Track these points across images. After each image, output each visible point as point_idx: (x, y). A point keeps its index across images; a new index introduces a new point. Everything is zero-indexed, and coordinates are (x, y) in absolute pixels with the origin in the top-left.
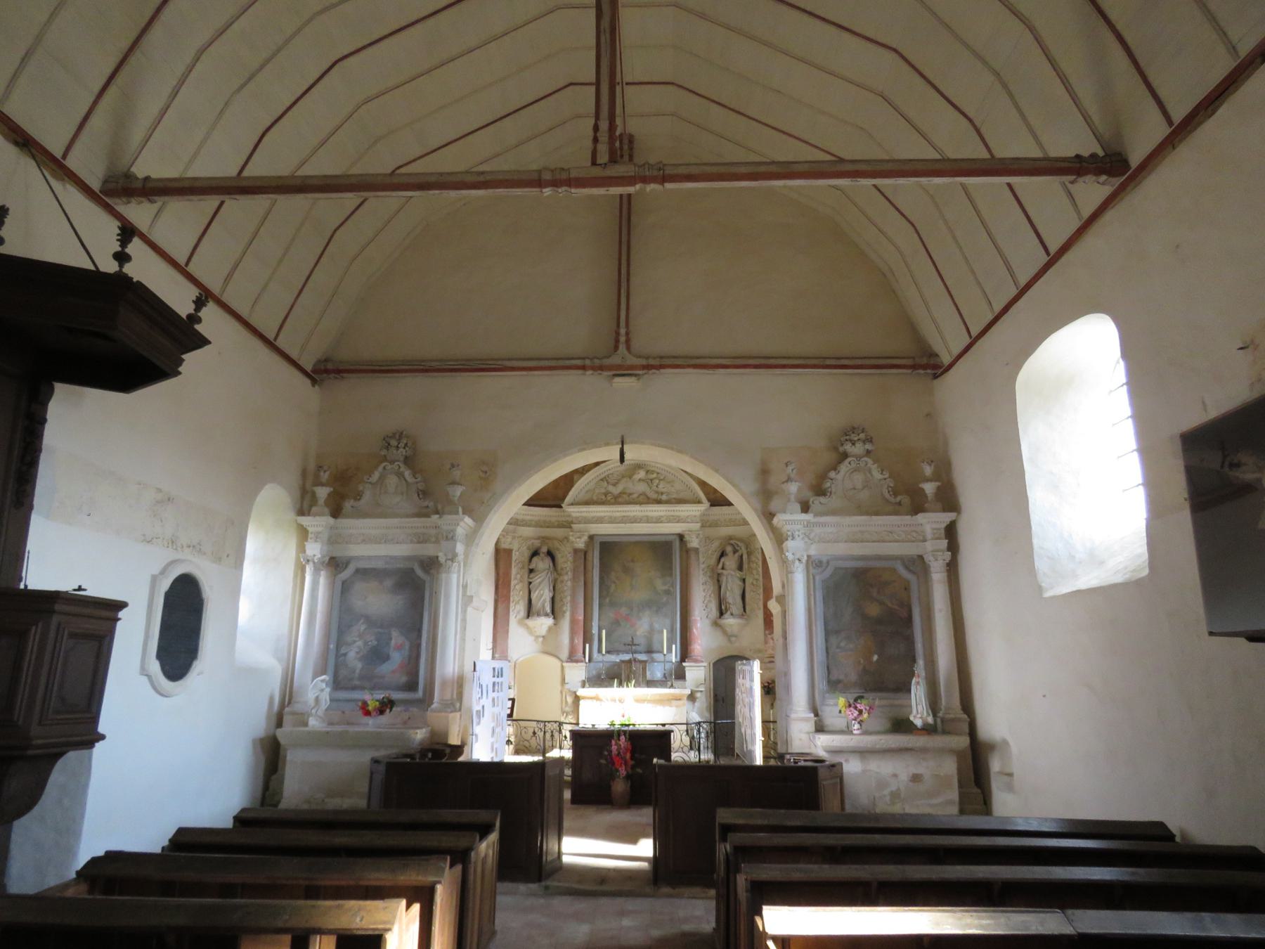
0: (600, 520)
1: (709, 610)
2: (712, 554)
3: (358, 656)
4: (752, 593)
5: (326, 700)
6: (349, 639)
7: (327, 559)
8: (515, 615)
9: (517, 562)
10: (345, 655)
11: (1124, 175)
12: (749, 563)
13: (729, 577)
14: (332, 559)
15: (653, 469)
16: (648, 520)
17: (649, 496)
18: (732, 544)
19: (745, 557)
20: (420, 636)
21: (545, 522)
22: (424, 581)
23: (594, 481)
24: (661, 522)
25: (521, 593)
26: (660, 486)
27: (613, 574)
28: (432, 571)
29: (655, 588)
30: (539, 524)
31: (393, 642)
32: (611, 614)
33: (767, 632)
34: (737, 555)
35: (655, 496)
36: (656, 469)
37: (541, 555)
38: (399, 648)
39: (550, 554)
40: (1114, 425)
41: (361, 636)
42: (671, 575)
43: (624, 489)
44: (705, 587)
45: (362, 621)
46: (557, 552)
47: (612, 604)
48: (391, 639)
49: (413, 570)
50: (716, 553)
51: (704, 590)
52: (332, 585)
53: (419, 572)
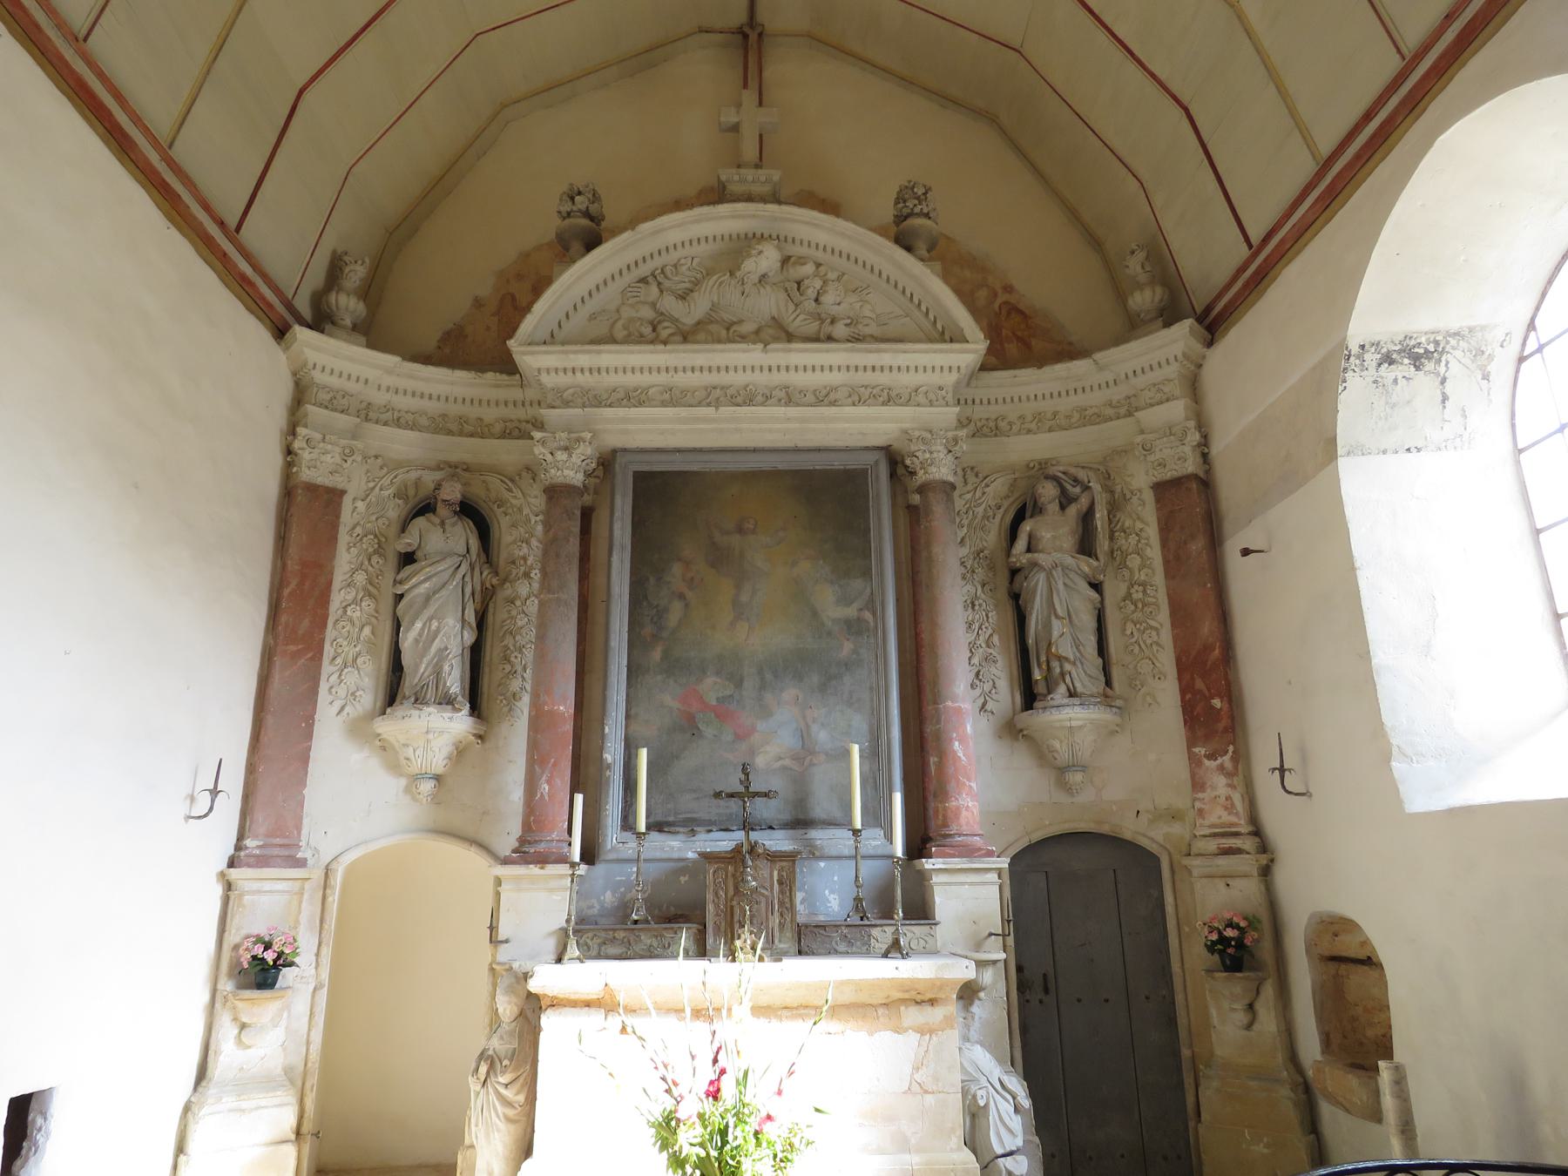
0: (634, 398)
1: (987, 687)
2: (986, 517)
4: (1130, 628)
8: (338, 704)
9: (359, 530)
12: (1112, 538)
13: (1057, 573)
18: (1055, 479)
19: (1100, 516)
21: (462, 420)
23: (621, 283)
24: (833, 403)
25: (367, 631)
26: (828, 299)
27: (677, 569)
29: (815, 614)
30: (441, 426)
32: (668, 698)
33: (1200, 750)
34: (1073, 510)
35: (812, 327)
36: (812, 252)
37: (442, 511)
39: (468, 510)
42: (866, 573)
43: (714, 307)
46: (499, 511)
47: (673, 666)
51: (970, 625)
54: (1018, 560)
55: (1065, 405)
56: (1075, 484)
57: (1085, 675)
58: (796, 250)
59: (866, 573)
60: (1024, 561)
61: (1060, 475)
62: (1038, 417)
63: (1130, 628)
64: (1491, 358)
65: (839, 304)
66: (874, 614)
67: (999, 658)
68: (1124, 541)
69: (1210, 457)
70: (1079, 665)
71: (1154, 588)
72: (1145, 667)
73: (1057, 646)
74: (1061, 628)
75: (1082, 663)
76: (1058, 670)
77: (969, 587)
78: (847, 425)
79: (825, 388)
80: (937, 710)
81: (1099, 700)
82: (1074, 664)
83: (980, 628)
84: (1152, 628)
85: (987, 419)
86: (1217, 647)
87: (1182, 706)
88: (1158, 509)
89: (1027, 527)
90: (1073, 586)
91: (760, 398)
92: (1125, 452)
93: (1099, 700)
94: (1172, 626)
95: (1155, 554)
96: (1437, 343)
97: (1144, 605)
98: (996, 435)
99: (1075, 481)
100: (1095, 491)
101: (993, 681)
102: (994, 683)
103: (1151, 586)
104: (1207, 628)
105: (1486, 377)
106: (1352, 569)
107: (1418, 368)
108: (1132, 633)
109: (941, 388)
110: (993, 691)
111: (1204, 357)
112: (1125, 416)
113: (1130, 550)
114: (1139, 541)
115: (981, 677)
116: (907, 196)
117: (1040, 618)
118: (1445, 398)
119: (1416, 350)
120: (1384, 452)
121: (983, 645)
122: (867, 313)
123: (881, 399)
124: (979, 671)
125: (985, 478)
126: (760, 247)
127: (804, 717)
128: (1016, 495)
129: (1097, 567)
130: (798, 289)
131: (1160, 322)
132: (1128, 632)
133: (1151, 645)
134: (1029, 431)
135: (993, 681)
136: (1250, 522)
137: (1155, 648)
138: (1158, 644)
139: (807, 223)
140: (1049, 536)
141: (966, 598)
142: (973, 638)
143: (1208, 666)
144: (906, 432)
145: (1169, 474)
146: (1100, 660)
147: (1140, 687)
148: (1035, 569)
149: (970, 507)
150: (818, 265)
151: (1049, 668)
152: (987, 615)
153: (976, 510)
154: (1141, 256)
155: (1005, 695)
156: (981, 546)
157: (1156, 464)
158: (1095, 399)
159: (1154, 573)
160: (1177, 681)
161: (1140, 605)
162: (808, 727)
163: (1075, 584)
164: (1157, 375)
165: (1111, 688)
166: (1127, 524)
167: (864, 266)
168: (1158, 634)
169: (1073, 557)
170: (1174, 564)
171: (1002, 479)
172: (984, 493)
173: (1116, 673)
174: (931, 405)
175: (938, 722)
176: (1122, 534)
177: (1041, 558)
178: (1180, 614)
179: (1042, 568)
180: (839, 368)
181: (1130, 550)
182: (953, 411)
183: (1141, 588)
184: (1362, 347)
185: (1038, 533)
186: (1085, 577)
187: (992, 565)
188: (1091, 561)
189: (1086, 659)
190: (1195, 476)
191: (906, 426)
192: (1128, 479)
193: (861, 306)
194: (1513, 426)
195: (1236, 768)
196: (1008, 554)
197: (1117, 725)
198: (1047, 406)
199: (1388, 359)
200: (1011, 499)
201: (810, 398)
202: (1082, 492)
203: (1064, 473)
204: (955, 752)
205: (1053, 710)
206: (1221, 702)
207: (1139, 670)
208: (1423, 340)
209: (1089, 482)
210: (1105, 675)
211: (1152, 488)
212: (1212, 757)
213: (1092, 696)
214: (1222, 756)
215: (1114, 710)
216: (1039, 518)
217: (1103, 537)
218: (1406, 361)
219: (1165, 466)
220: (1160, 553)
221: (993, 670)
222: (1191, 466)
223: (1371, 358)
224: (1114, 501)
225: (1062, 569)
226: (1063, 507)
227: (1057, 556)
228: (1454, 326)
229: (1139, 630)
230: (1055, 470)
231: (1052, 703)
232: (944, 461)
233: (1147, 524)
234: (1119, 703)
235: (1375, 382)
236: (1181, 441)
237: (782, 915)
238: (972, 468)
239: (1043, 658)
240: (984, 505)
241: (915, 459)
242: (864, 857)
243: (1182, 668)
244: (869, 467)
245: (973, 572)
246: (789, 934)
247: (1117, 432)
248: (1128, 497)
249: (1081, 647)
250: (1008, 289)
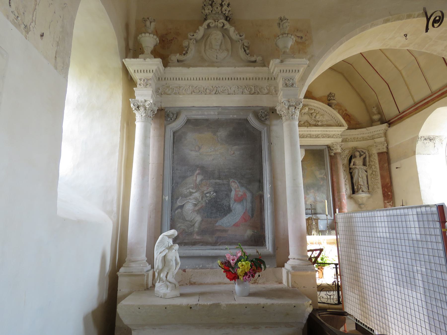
3: (197, 208)
4: (372, 179)
5: (176, 260)
6: (185, 191)
7: (156, 109)
10: (182, 207)
11: (439, 22)
13: (360, 169)
14: (161, 110)
15: (312, 107)
16: (311, 136)
17: (310, 123)
18: (359, 151)
19: (367, 158)
20: (261, 188)
22: (260, 133)
24: (319, 138)
26: (317, 117)
28: (267, 122)
31: (233, 194)
33: (386, 202)
34: (362, 157)
35: (314, 123)
36: (314, 108)
38: (240, 200)
41: (197, 187)
42: (325, 169)
45: (197, 172)
48: (231, 191)
49: (247, 120)
50: (347, 157)
52: (162, 137)
53: (254, 122)
55: (359, 136)
57: (365, 188)
58: (311, 107)
59: (325, 169)
60: (354, 167)
62: (354, 138)
63: (372, 179)
64: (443, 141)
65: (319, 118)
66: (326, 176)
72: (375, 186)
76: (360, 187)
78: (322, 142)
79: (317, 134)
82: (363, 186)
84: (377, 179)
85: (344, 139)
89: (353, 160)
91: (305, 137)
95: (377, 166)
96: (434, 138)
97: (375, 175)
98: (346, 142)
104: (388, 180)
105: (442, 144)
106: (418, 174)
107: (430, 141)
109: (338, 135)
111: (388, 129)
112: (372, 139)
114: (374, 163)
116: (331, 96)
118: (435, 146)
119: (430, 138)
120: (424, 154)
122: (324, 120)
123: (327, 137)
125: (344, 150)
126: (305, 108)
127: (315, 195)
130: (311, 115)
131: (379, 123)
132: (372, 180)
134: (352, 141)
138: (378, 182)
139: (313, 103)
140: (358, 162)
144: (332, 143)
145: (380, 151)
148: (356, 169)
150: (315, 110)
152: (345, 176)
154: (376, 108)
155: (349, 191)
157: (378, 149)
158: (366, 135)
159: (377, 169)
161: (374, 175)
162: (315, 197)
164: (379, 132)
166: (372, 160)
167: (324, 111)
168: (378, 181)
170: (381, 168)
173: (370, 187)
174: (337, 138)
175: (340, 196)
177: (357, 167)
178: (382, 177)
179: (357, 168)
180: (320, 131)
182: (340, 140)
184: (421, 137)
191: (333, 142)
192: (372, 151)
193: (323, 118)
194: (446, 152)
195: (393, 205)
198: (356, 136)
199: (426, 139)
200: (349, 154)
201: (314, 137)
204: (343, 202)
208: (432, 137)
212: (388, 203)
213: (366, 192)
214: (390, 203)
215: (370, 194)
218: (429, 140)
219: (380, 150)
220: (378, 166)
222: (385, 150)
223: (423, 139)
226: (360, 157)
228: (437, 135)
230: (359, 150)
231: (359, 193)
233: (376, 160)
235: (423, 143)
237: (316, 229)
242: (328, 219)
246: (317, 232)
247: (370, 142)
249: (364, 183)
250: (346, 110)
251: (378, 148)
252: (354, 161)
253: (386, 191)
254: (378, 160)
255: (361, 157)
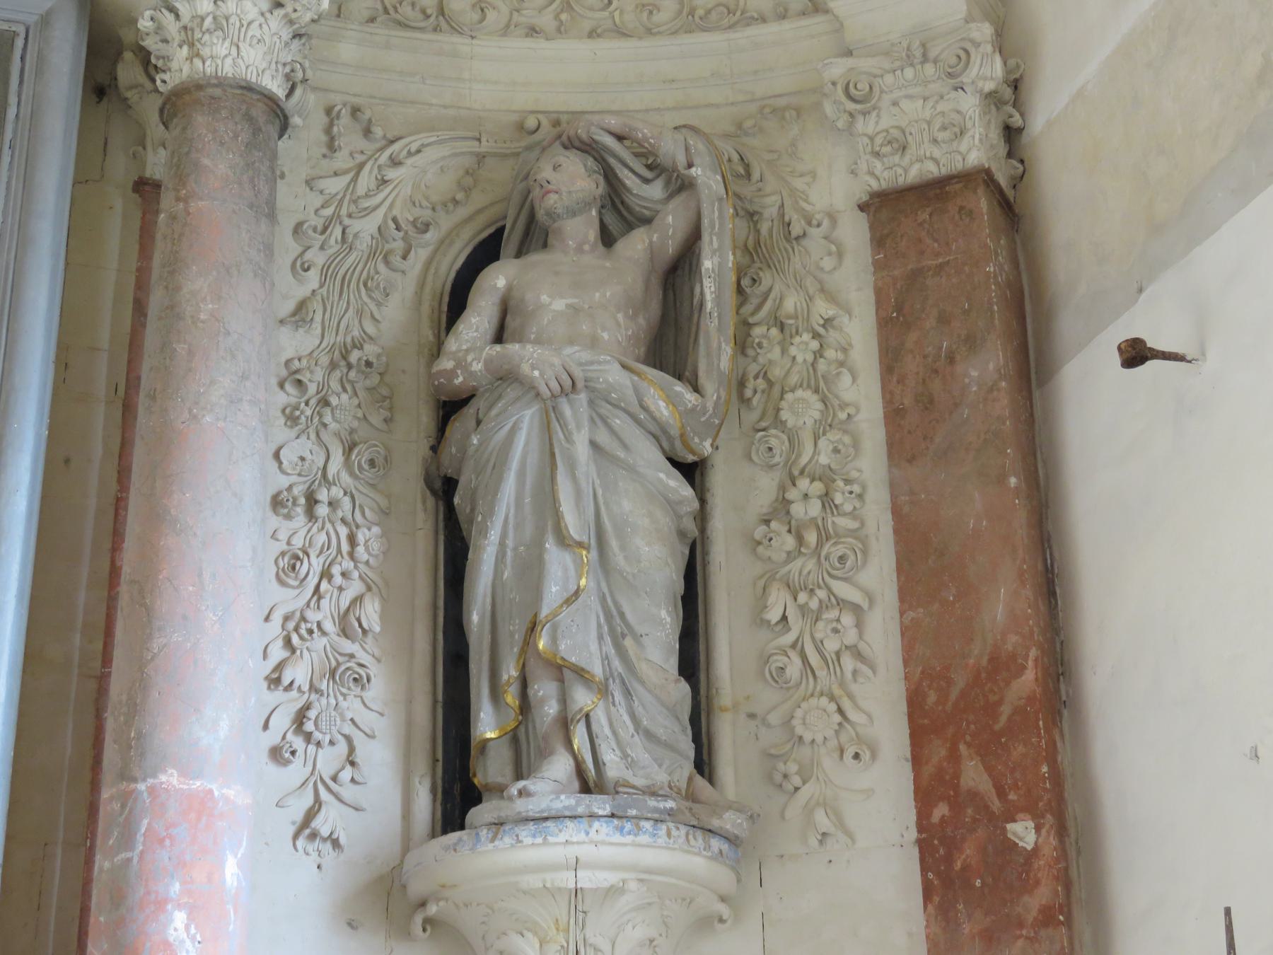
1: (328, 760)
2: (380, 252)
12: (742, 344)
13: (575, 411)
18: (588, 148)
34: (636, 245)
40: (757, 739)
44: (296, 528)
51: (291, 564)
54: (461, 364)
56: (648, 174)
61: (609, 141)
63: (778, 602)
67: (374, 669)
68: (776, 353)
69: (1025, 138)
70: (618, 697)
71: (856, 488)
73: (555, 629)
74: (572, 572)
75: (628, 693)
76: (551, 709)
77: (299, 448)
80: (126, 798)
81: (670, 804)
82: (603, 691)
83: (326, 574)
84: (842, 603)
86: (1030, 663)
87: (920, 842)
88: (878, 266)
89: (497, 279)
90: (621, 454)
92: (799, 111)
93: (670, 804)
94: (902, 599)
97: (824, 537)
98: (436, 29)
99: (650, 167)
100: (704, 193)
101: (348, 739)
102: (352, 749)
103: (847, 482)
108: (784, 618)
110: (346, 774)
113: (794, 379)
114: (819, 354)
115: (309, 726)
117: (510, 543)
121: (329, 626)
124: (307, 707)
128: (479, 199)
129: (693, 409)
132: (774, 615)
133: (838, 654)
134: (533, 31)
135: (348, 739)
136: (1140, 291)
137: (848, 663)
138: (858, 655)
140: (559, 305)
141: (294, 479)
142: (301, 602)
143: (1003, 719)
145: (914, 171)
146: (685, 687)
147: (797, 781)
148: (511, 392)
149: (336, 217)
151: (525, 706)
152: (352, 540)
153: (356, 226)
156: (356, 333)
157: (879, 140)
159: (856, 445)
160: (908, 767)
161: (811, 537)
163: (625, 446)
165: (711, 780)
166: (790, 304)
168: (859, 625)
169: (624, 366)
171: (444, 151)
172: (384, 182)
176: (774, 332)
181: (794, 379)
183: (818, 487)
185: (529, 296)
186: (658, 434)
187: (384, 391)
188: (679, 387)
189: (642, 682)
190: (984, 177)
192: (799, 184)
196: (437, 350)
197: (723, 899)
200: (462, 212)
202: (670, 197)
203: (620, 138)
205: (525, 833)
206: (1038, 829)
207: (799, 730)
209: (690, 166)
210: (697, 739)
211: (862, 207)
215: (716, 843)
216: (535, 258)
217: (720, 329)
221: (352, 706)
224: (758, 243)
225: (591, 403)
226: (607, 239)
227: (575, 355)
229: (803, 609)
232: (254, 30)
234: (730, 821)
236: (950, 75)
238: (355, 111)
239: (510, 671)
240: (381, 212)
241: (170, 17)
243: (920, 734)
244: (21, 30)
245: (325, 402)
248: (796, 230)
249: (628, 642)
251: (886, 122)
252: (509, 288)
253: (974, 795)
254: (879, 293)
255: (620, 246)
